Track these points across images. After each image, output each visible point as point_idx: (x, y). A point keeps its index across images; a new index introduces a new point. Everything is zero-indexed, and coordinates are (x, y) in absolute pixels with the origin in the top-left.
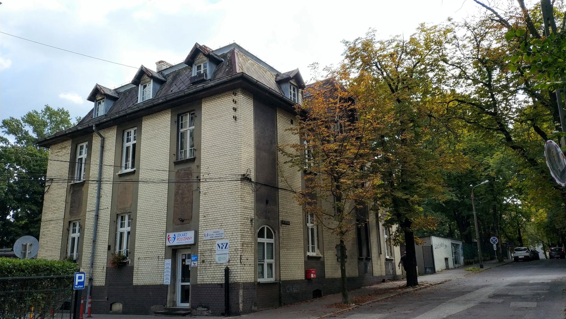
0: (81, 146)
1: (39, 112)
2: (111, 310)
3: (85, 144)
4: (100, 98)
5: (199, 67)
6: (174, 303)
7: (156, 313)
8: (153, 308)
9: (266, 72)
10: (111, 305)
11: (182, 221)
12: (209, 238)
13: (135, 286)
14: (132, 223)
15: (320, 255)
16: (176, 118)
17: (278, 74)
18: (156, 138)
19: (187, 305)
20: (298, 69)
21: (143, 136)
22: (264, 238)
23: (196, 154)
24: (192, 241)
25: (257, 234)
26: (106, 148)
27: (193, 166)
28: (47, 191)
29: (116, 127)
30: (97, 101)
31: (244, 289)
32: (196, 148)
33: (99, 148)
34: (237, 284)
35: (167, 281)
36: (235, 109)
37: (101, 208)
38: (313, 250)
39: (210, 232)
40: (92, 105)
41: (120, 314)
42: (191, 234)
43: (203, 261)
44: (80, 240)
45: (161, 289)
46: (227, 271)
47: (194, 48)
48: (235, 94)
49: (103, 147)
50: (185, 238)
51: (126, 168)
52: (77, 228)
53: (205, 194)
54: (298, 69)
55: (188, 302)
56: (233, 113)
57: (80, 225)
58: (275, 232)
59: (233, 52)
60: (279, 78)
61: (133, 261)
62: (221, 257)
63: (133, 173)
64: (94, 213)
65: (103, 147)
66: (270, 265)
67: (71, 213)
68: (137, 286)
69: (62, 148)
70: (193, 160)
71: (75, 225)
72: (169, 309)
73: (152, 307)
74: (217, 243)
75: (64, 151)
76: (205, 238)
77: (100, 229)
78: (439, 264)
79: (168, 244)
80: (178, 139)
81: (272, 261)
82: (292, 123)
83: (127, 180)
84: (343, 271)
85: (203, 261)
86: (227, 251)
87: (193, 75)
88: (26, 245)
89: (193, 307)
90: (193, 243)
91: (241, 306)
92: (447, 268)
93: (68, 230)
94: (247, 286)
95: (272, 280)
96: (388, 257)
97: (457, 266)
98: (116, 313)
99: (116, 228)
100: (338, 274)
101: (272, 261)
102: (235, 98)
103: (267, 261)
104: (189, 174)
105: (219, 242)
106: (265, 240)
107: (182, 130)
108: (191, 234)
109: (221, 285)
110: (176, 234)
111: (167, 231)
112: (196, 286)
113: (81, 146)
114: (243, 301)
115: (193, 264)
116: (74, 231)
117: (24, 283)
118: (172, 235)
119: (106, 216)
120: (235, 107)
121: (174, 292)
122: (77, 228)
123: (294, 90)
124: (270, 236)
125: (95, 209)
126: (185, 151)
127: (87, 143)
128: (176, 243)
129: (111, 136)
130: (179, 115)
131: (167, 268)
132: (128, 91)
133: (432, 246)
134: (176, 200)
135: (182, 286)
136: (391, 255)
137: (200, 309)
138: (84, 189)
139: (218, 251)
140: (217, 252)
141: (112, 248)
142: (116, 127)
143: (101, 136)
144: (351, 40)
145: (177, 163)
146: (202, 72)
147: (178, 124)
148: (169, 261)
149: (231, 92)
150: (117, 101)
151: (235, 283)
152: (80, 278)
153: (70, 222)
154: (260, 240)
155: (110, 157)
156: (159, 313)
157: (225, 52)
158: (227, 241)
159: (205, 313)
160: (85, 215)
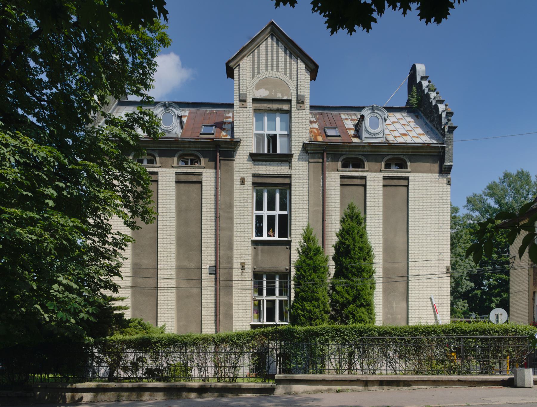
1: (497, 181)
88: (498, 315)
117: (500, 340)
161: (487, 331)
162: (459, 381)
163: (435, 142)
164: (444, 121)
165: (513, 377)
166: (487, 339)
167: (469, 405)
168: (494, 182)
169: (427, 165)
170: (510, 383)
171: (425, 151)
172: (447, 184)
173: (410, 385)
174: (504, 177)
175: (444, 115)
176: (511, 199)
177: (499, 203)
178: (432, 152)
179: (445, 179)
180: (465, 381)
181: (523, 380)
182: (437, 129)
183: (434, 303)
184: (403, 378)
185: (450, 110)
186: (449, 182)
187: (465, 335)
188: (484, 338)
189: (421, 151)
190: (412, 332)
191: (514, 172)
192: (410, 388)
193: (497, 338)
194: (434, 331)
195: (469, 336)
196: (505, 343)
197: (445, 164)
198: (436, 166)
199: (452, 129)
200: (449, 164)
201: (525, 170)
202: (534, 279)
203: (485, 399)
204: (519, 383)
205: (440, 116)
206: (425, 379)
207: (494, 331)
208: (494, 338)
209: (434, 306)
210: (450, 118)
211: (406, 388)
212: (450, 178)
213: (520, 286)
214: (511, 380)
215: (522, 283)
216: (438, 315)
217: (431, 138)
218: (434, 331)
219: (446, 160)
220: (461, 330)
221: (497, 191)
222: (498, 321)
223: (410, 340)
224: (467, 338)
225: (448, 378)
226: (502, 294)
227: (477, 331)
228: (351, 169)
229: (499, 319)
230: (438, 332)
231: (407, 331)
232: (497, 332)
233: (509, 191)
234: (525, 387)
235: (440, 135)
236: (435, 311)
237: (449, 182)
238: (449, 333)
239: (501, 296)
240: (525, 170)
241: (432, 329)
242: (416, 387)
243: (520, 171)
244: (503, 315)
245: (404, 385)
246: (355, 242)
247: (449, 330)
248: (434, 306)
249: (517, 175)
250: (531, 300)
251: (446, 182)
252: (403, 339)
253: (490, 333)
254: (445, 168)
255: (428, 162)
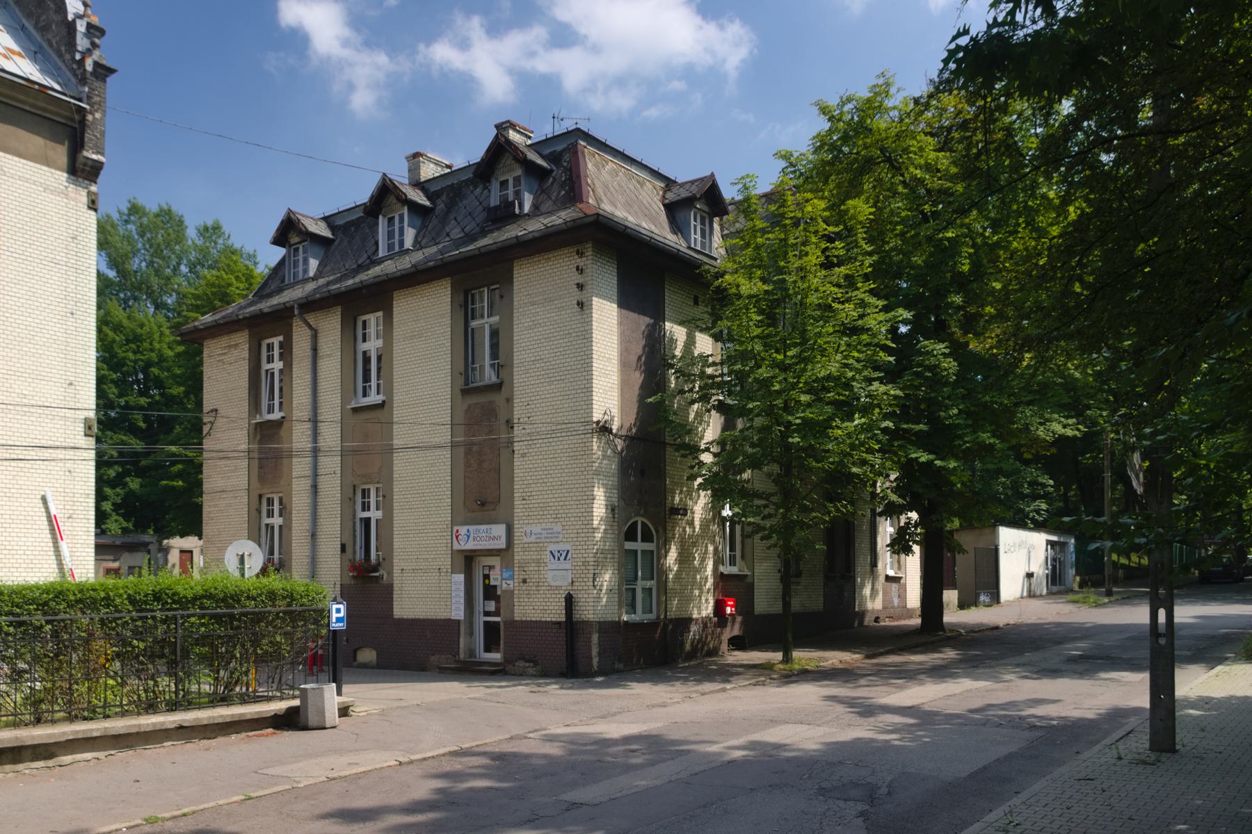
0: (268, 345)
1: (115, 216)
2: (355, 659)
3: (276, 341)
4: (296, 239)
5: (504, 184)
6: (472, 653)
7: (440, 668)
8: (434, 659)
9: (642, 184)
10: (355, 652)
11: (483, 504)
12: (533, 539)
13: (399, 620)
14: (386, 502)
15: (746, 572)
16: (461, 298)
17: (669, 183)
18: (421, 338)
19: (496, 656)
20: (712, 175)
21: (398, 331)
22: (636, 540)
23: (503, 373)
24: (502, 544)
25: (622, 536)
26: (320, 353)
27: (499, 399)
28: (209, 433)
29: (339, 309)
30: (290, 246)
31: (599, 632)
32: (502, 362)
33: (309, 352)
34: (587, 623)
35: (458, 613)
36: (580, 287)
37: (320, 471)
38: (733, 562)
39: (536, 529)
40: (280, 252)
41: (373, 667)
42: (499, 530)
43: (524, 581)
44: (285, 531)
45: (450, 626)
46: (569, 600)
47: (493, 143)
48: (580, 254)
49: (315, 350)
50: (490, 536)
51: (365, 395)
52: (276, 507)
53: (524, 455)
54: (712, 175)
55: (498, 651)
56: (576, 295)
57: (281, 503)
58: (657, 531)
59: (573, 151)
60: (671, 196)
61: (390, 573)
62: (558, 577)
63: (382, 405)
64: (307, 483)
65: (315, 350)
66: (648, 591)
67: (262, 478)
68: (401, 621)
69: (230, 347)
70: (498, 387)
71: (270, 502)
72: (464, 662)
73: (433, 658)
74: (549, 549)
75: (235, 353)
76: (525, 540)
77: (322, 512)
78: (1011, 584)
79: (456, 547)
80: (467, 341)
81: (649, 584)
82: (696, 303)
83: (369, 419)
84: (786, 605)
85: (524, 581)
86: (567, 565)
87: (492, 205)
88: (242, 556)
89: (508, 660)
90: (504, 546)
91: (595, 661)
92: (1031, 595)
93: (259, 511)
94: (610, 629)
95: (652, 616)
96: (891, 573)
97: (1055, 589)
98: (365, 666)
99: (355, 511)
100: (777, 608)
101: (649, 584)
102: (581, 262)
103: (640, 585)
104: (490, 413)
105: (554, 548)
106: (639, 546)
107: (474, 324)
108: (499, 530)
109: (559, 623)
110: (472, 528)
111: (453, 523)
112: (512, 624)
113: (268, 345)
114: (599, 654)
115: (504, 585)
116: (270, 514)
117: (258, 617)
118: (463, 530)
119: (332, 488)
120: (580, 281)
121: (471, 633)
122: (276, 507)
123: (703, 223)
124: (647, 538)
125: (309, 473)
126: (482, 367)
127: (281, 338)
128: (471, 545)
129: (330, 326)
130: (466, 294)
131: (458, 589)
132: (351, 223)
133: (996, 550)
134: (467, 465)
135: (486, 623)
136: (899, 568)
137: (521, 664)
138: (283, 432)
139: (553, 564)
140: (550, 566)
141: (349, 549)
142: (339, 309)
143: (310, 327)
144: (833, 102)
145: (466, 392)
146: (511, 198)
147: (465, 309)
148: (460, 578)
149: (573, 249)
150: (333, 247)
151: (583, 622)
152: (338, 611)
153: (260, 496)
154: (629, 545)
155: (331, 367)
156: (447, 669)
157: (559, 148)
158: (567, 547)
159: (531, 671)
160: (290, 484)
161: (232, 597)
162: (181, 727)
163: (57, 87)
164: (82, 43)
165: (296, 702)
166: (232, 617)
167: (250, 798)
168: (108, 216)
169: (37, 142)
170: (290, 721)
171: (31, 100)
172: (90, 208)
173: (51, 756)
174: (129, 210)
175: (81, 27)
176: (144, 264)
177: (117, 267)
178: (51, 112)
179: (84, 193)
180: (192, 728)
181: (322, 712)
182: (60, 56)
183: (53, 511)
184: (33, 737)
185: (95, 20)
186: (93, 202)
187: (183, 609)
188: (224, 615)
189: (22, 97)
190: (46, 604)
191: (151, 206)
192: (50, 763)
193: (253, 613)
194: (107, 598)
195: (191, 611)
196: (269, 623)
197: (85, 153)
198: (61, 153)
199: (103, 71)
200: (94, 157)
201: (177, 209)
202: (261, 467)
203: (271, 771)
204: (312, 720)
205: (71, 27)
206: (95, 734)
207: (248, 598)
208: (245, 614)
209: (52, 522)
210: (97, 41)
211: (41, 764)
212: (95, 194)
213: (229, 478)
214: (293, 711)
215: (232, 471)
216: (63, 545)
217: (42, 71)
218: (107, 598)
219: (88, 144)
220: (174, 594)
221: (115, 240)
222: (243, 575)
223: (42, 626)
224: (189, 616)
225: (154, 724)
226: (128, 479)
227: (210, 597)
228: (712, 270)
229: (247, 566)
230: (118, 601)
231: (33, 601)
232: (254, 599)
233: (140, 245)
234: (324, 728)
235: (69, 74)
236: (55, 532)
237: (93, 202)
238: (146, 603)
239: (125, 485)
240: (174, 209)
241: (103, 594)
242: (67, 759)
243: (166, 207)
244: (254, 557)
245: (36, 758)
246: (164, 388)
247: (146, 595)
248: (52, 522)
249: (157, 215)
250: (254, 513)
251: (85, 199)
252: (21, 624)
253: (238, 601)
254: (85, 165)
255: (38, 134)
